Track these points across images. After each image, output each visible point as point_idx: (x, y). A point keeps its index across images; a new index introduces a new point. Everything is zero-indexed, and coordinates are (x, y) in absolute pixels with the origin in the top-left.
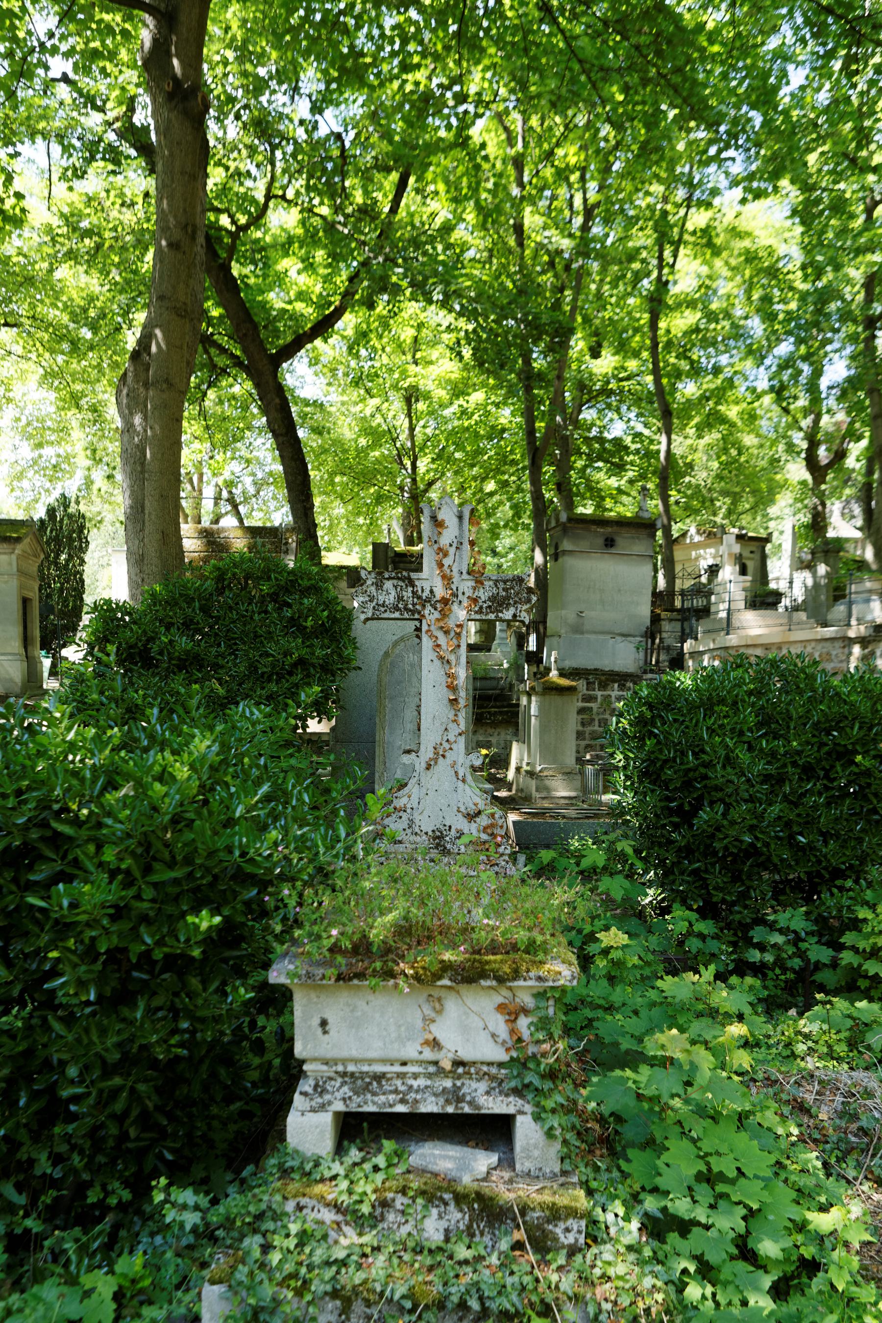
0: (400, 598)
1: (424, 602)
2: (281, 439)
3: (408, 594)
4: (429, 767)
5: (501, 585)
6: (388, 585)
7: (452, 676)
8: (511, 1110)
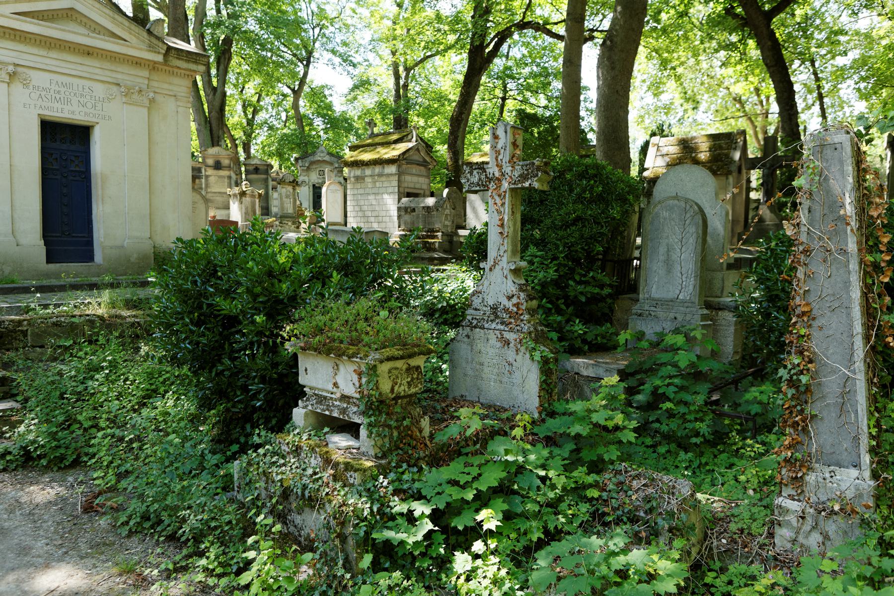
0: (480, 179)
1: (490, 180)
2: (772, 69)
3: (483, 177)
4: (491, 270)
5: (525, 168)
6: (475, 172)
7: (502, 220)
8: (359, 421)
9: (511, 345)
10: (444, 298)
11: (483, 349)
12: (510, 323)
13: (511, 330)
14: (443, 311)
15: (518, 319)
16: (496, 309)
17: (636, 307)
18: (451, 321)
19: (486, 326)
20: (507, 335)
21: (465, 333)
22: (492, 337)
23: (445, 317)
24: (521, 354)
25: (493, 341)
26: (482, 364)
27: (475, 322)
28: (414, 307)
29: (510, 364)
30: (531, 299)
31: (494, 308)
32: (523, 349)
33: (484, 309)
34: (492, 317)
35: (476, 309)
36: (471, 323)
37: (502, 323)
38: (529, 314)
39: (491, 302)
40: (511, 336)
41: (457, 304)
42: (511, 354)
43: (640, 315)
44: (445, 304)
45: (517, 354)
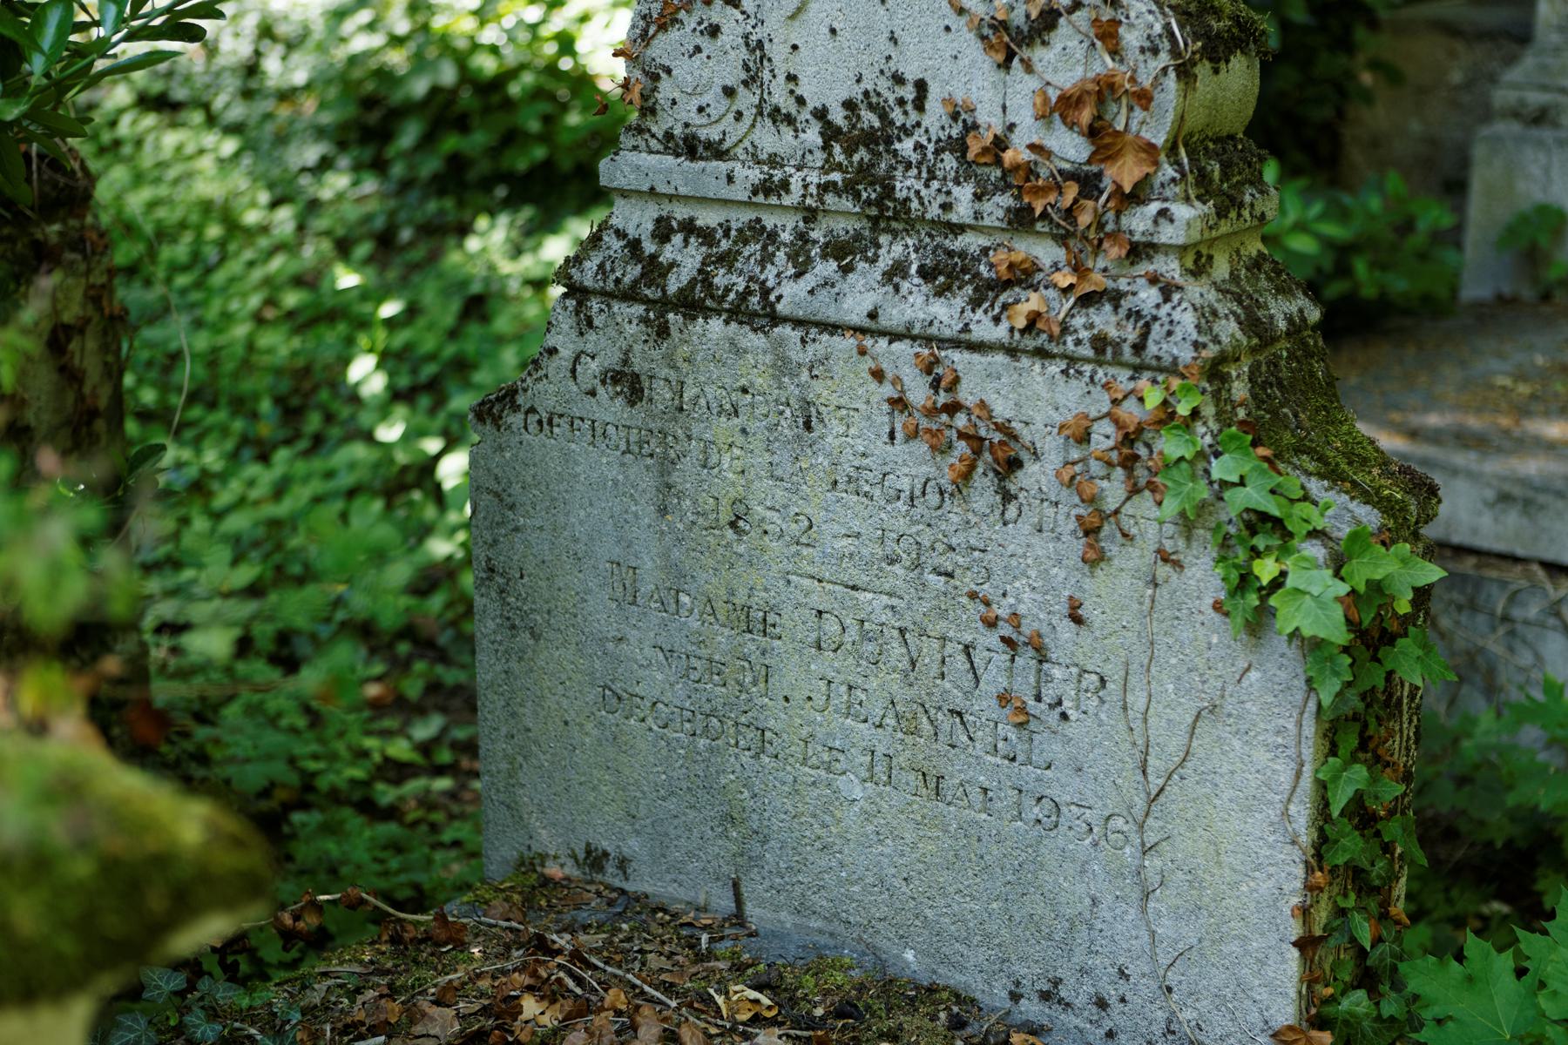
9: (1035, 476)
10: (444, 42)
11: (764, 497)
12: (1024, 276)
13: (1036, 342)
14: (442, 113)
15: (1102, 235)
16: (881, 139)
17: (1514, 74)
18: (484, 167)
19: (792, 295)
20: (996, 387)
21: (604, 351)
22: (852, 396)
23: (451, 142)
24: (1129, 562)
25: (857, 425)
26: (757, 622)
27: (685, 259)
28: (287, 95)
29: (1022, 644)
30: (1217, 50)
31: (864, 140)
32: (1150, 519)
33: (768, 139)
34: (843, 217)
35: (691, 147)
36: (655, 270)
37: (943, 274)
38: (1204, 188)
39: (828, 83)
40: (1036, 400)
41: (512, 74)
42: (1029, 556)
43: (1541, 117)
44: (448, 75)
45: (1095, 559)
